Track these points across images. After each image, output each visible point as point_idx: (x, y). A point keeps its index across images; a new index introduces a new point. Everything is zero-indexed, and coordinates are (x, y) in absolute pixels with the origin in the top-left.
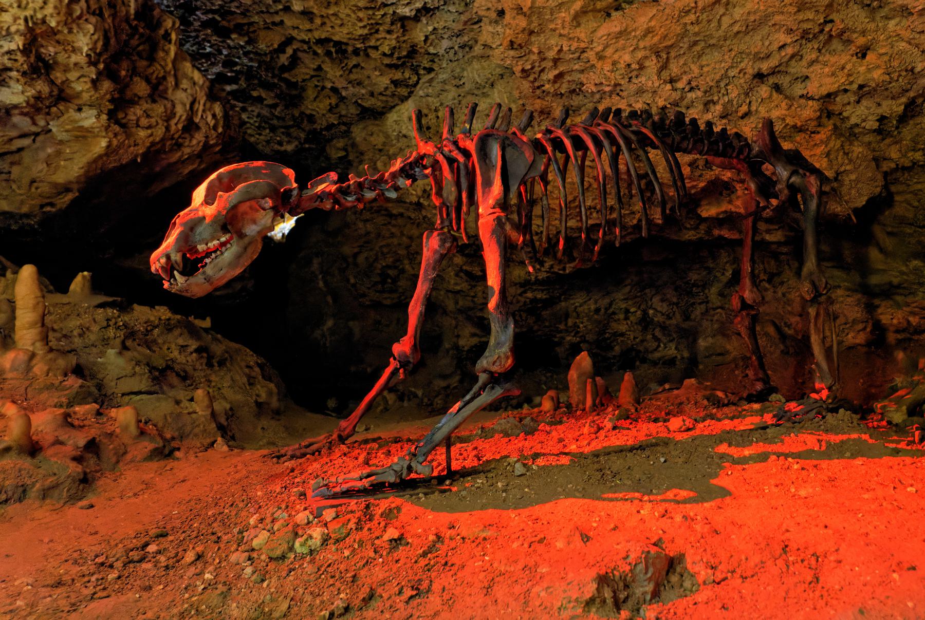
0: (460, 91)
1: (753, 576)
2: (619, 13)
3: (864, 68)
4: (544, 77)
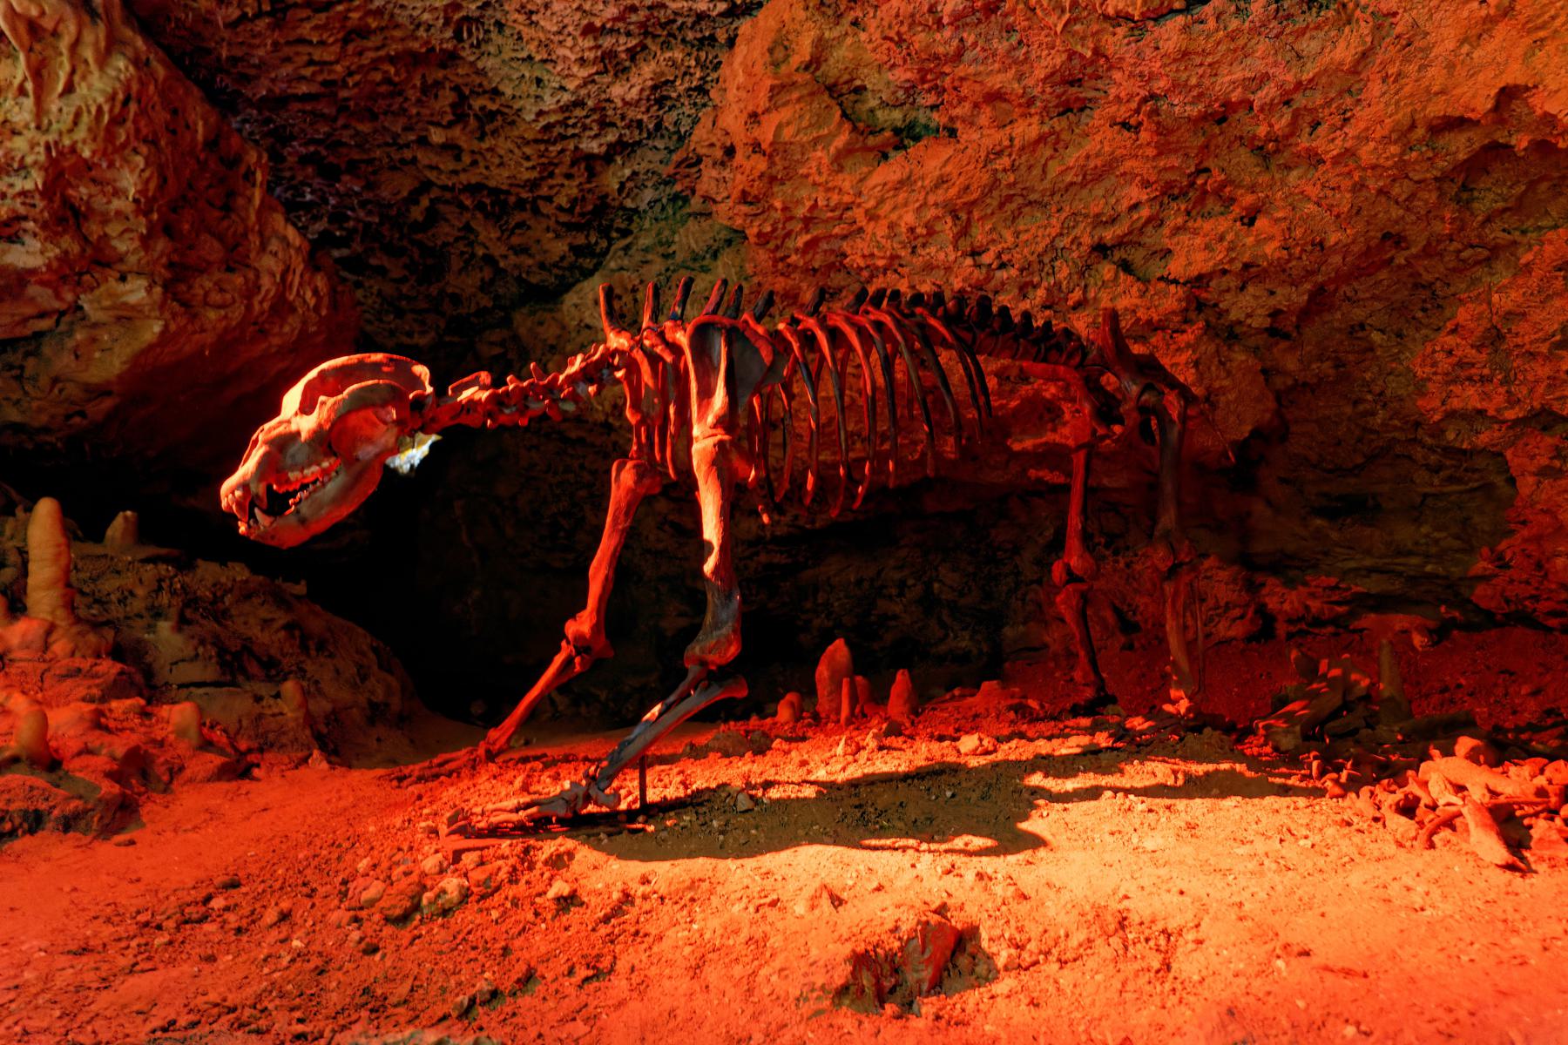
4: (790, 244)
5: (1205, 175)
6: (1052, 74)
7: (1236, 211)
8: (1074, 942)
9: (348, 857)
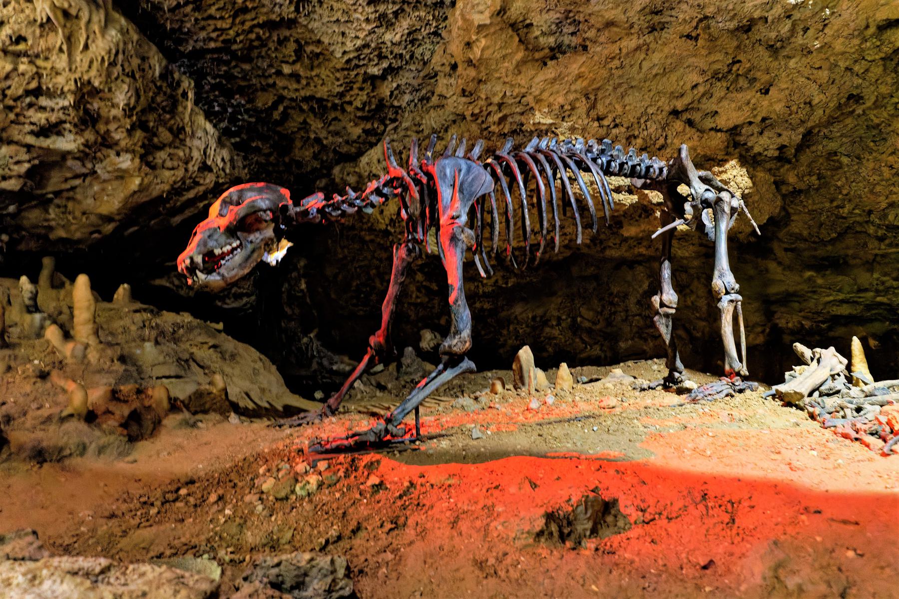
0: (420, 135)
1: (677, 518)
2: (554, 62)
3: (767, 102)
4: (490, 119)
5: (737, 65)
6: (644, 8)
7: (758, 86)
8: (676, 507)
9: (254, 465)
